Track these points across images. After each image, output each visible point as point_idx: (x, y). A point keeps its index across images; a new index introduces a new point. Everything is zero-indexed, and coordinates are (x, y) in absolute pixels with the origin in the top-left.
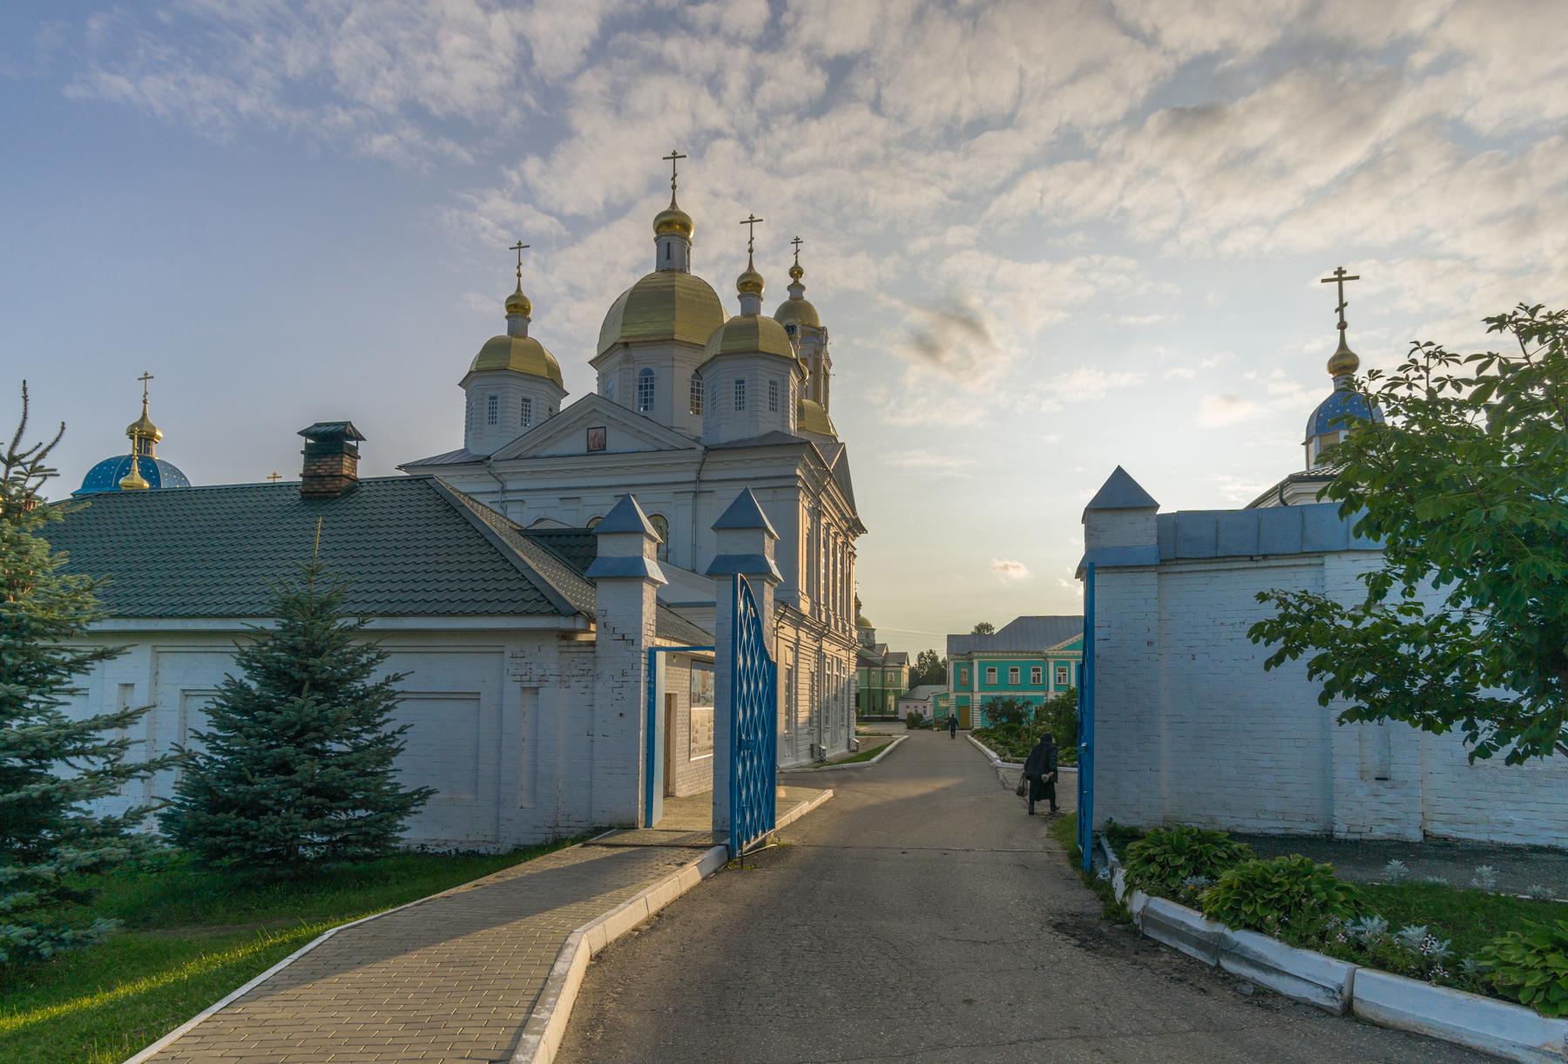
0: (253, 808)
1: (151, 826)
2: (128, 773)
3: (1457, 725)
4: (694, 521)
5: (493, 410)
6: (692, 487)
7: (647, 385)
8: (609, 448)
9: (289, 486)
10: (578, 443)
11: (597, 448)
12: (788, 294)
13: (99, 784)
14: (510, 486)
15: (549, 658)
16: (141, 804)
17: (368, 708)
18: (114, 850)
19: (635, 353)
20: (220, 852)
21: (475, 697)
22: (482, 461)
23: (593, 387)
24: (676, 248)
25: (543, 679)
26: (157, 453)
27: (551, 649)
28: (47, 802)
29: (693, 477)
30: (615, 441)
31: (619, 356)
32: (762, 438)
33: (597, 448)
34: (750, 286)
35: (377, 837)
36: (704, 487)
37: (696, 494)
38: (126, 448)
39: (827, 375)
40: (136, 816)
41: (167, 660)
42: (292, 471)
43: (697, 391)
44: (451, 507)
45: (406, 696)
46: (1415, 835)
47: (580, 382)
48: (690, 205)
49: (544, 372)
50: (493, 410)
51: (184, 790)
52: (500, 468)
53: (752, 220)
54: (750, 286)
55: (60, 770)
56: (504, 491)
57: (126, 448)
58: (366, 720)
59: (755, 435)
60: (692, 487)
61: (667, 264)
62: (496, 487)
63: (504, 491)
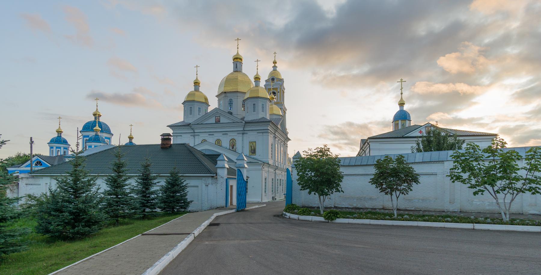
3: (308, 190)
4: (243, 141)
5: (191, 110)
6: (242, 132)
7: (231, 103)
8: (221, 122)
9: (159, 145)
10: (213, 120)
11: (218, 122)
14: (196, 131)
15: (210, 180)
19: (228, 95)
21: (197, 186)
22: (189, 125)
23: (216, 106)
24: (238, 65)
25: (209, 184)
26: (101, 120)
27: (210, 179)
29: (242, 129)
30: (223, 120)
31: (223, 95)
33: (218, 122)
34: (257, 79)
36: (245, 132)
37: (243, 134)
38: (93, 119)
39: (284, 92)
42: (159, 142)
43: (243, 105)
45: (189, 187)
46: (333, 206)
47: (214, 104)
48: (242, 53)
49: (204, 101)
50: (191, 110)
53: (258, 61)
54: (257, 79)
57: (93, 119)
58: (183, 190)
60: (242, 132)
61: (236, 70)
62: (192, 131)
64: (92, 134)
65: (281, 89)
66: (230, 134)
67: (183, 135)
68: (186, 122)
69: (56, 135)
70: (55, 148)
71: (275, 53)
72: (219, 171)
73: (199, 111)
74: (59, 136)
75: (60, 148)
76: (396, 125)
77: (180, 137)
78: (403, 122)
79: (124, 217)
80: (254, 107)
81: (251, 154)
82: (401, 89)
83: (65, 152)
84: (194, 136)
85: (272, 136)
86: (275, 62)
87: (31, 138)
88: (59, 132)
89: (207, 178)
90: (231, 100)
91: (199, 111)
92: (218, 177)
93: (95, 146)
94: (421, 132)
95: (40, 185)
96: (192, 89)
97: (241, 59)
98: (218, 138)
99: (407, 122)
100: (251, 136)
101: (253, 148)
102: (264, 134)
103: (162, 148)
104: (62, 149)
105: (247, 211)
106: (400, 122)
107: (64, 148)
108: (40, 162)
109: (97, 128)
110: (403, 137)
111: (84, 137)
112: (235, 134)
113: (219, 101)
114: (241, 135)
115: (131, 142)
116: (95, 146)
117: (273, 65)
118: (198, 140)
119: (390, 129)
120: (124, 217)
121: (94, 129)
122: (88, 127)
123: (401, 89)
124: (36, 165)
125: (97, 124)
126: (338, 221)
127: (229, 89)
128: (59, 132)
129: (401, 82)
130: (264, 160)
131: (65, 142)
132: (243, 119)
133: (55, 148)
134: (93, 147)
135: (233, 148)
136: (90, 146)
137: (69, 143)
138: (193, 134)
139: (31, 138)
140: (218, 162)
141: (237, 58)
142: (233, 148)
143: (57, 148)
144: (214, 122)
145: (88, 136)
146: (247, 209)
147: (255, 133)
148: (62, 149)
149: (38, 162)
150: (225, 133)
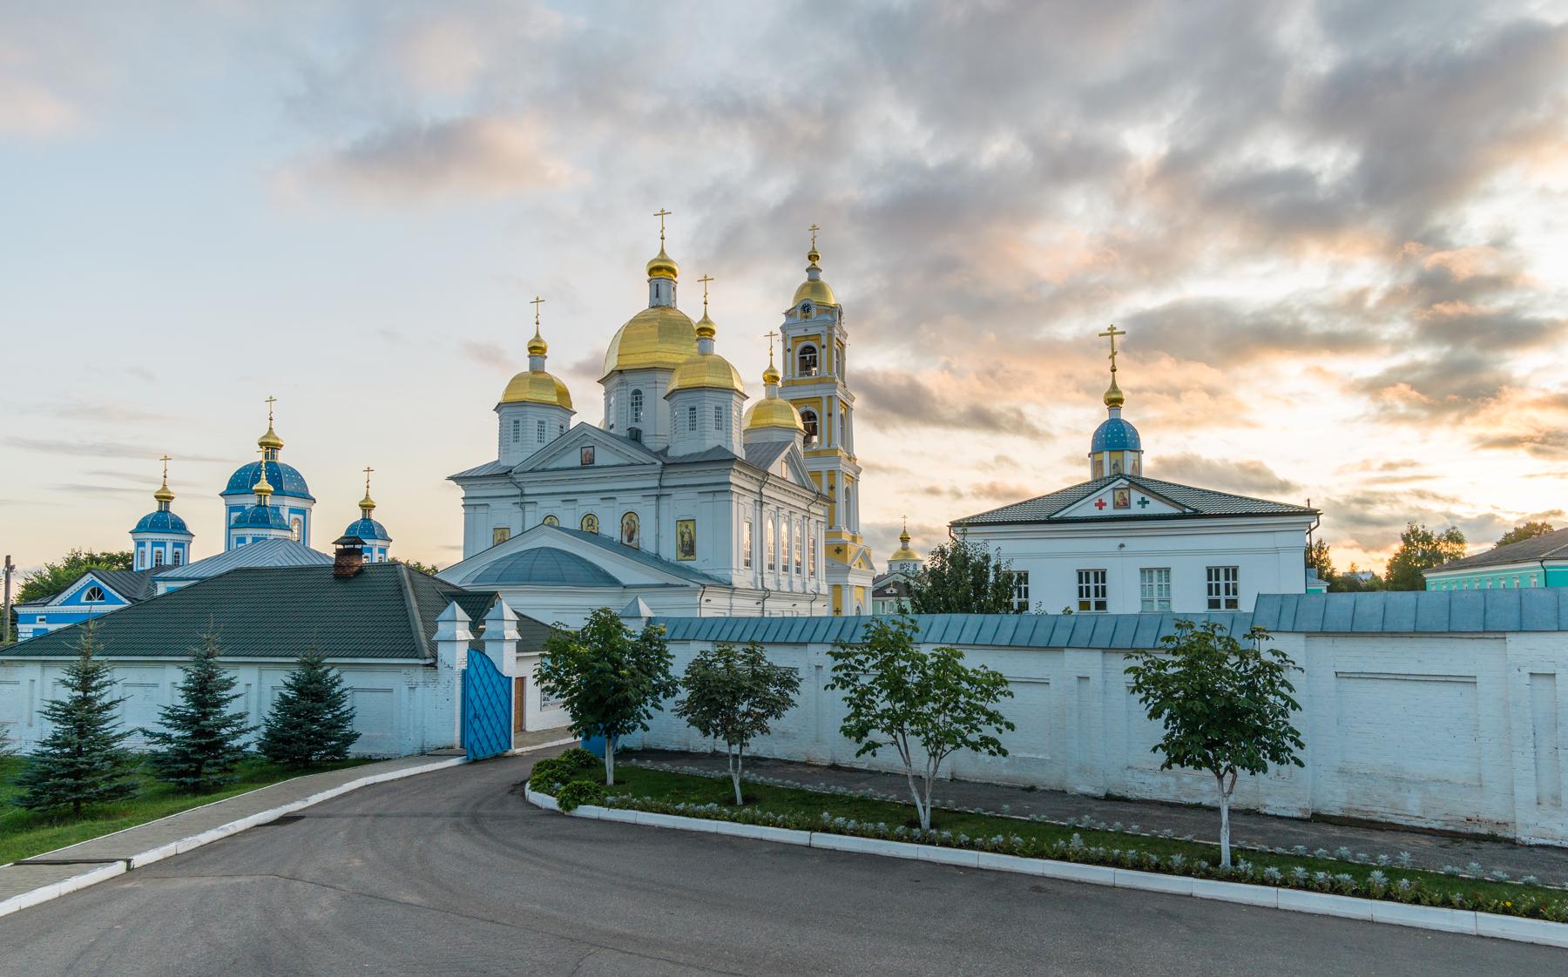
0: (288, 741)
1: (253, 748)
2: (244, 732)
4: (658, 517)
5: (516, 430)
8: (597, 463)
10: (573, 459)
11: (588, 463)
12: (806, 275)
13: (234, 735)
14: (527, 491)
15: (419, 676)
16: (250, 742)
17: (335, 702)
18: (239, 755)
19: (629, 378)
20: (277, 758)
24: (663, 289)
26: (282, 458)
27: (420, 671)
28: (221, 742)
29: (656, 484)
31: (616, 380)
32: (708, 452)
33: (588, 463)
35: (338, 751)
37: (658, 497)
38: (258, 456)
40: (247, 745)
41: (265, 673)
44: (400, 589)
47: (591, 407)
50: (516, 430)
51: (266, 735)
52: (519, 478)
55: (224, 731)
56: (523, 495)
57: (258, 456)
59: (703, 450)
62: (518, 492)
63: (523, 495)
64: (250, 501)
65: (830, 336)
66: (621, 497)
67: (494, 504)
68: (504, 464)
69: (153, 507)
70: (148, 545)
71: (814, 228)
72: (442, 650)
73: (541, 431)
74: (164, 512)
75: (163, 544)
76: (1097, 466)
77: (483, 510)
78: (1117, 456)
79: (102, 797)
80: (693, 418)
81: (681, 555)
82: (1112, 357)
83: (176, 556)
84: (522, 505)
85: (749, 499)
86: (813, 257)
87: (8, 558)
88: (164, 499)
89: (412, 670)
90: (637, 392)
91: (541, 431)
92: (439, 665)
93: (255, 540)
94: (1101, 505)
95: (17, 683)
96: (525, 367)
97: (672, 271)
98: (588, 510)
99: (1129, 457)
100: (682, 504)
101: (686, 537)
102: (719, 497)
103: (337, 577)
104: (169, 546)
105: (515, 756)
106: (1106, 455)
107: (175, 545)
108: (100, 591)
109: (264, 484)
110: (1049, 521)
111: (231, 509)
112: (637, 497)
113: (608, 394)
114: (653, 501)
115: (366, 520)
116: (255, 540)
117: (810, 263)
118: (533, 517)
119: (1085, 474)
120: (102, 797)
121: (263, 488)
122: (241, 482)
123: (1112, 357)
124: (89, 598)
125: (263, 476)
126: (588, 811)
127: (633, 361)
128: (164, 499)
129: (1112, 334)
130: (718, 574)
131: (179, 526)
132: (664, 452)
133: (148, 545)
134: (249, 540)
135: (630, 539)
136: (241, 540)
137: (190, 529)
138: (517, 500)
139: (8, 558)
140: (441, 626)
141: (659, 269)
142: (630, 539)
143: (155, 544)
144: (578, 464)
145: (241, 508)
146: (510, 752)
147: (692, 494)
148: (169, 546)
149: (93, 591)
150: (608, 496)
